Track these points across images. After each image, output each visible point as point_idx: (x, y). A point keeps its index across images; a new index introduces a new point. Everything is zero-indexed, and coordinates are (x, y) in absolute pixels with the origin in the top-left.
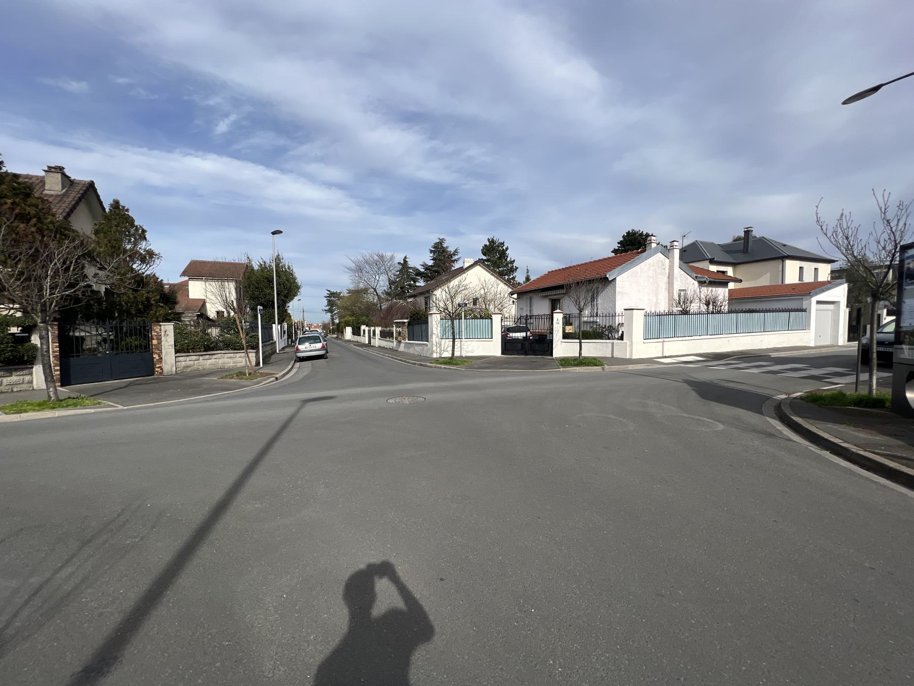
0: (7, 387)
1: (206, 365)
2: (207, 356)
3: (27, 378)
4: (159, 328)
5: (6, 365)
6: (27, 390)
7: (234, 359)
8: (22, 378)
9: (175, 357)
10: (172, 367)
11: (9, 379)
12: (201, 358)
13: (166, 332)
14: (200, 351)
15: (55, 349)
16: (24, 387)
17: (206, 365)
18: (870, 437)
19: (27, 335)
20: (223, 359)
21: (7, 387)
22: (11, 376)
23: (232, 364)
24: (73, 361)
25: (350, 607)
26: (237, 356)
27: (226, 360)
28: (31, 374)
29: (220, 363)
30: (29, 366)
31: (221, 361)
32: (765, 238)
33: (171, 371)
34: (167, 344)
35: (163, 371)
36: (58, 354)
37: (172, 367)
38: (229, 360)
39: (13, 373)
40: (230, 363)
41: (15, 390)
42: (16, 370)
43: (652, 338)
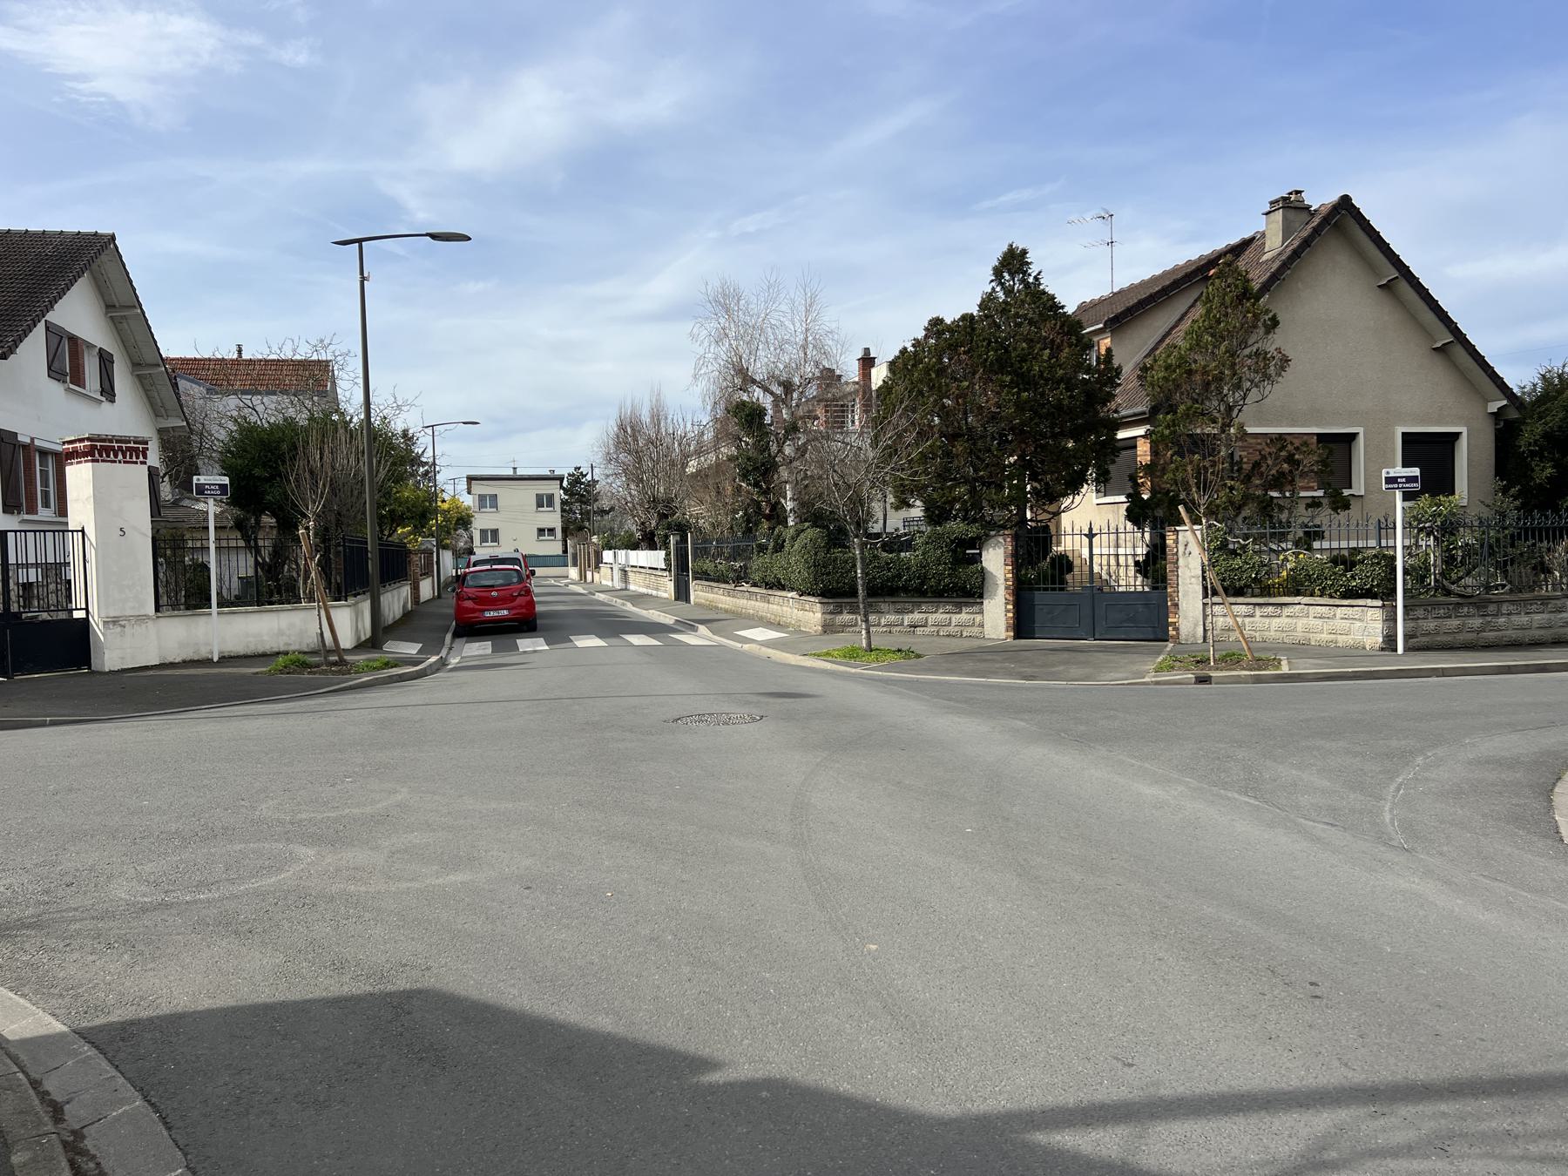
0: (957, 629)
1: (1269, 629)
2: (1271, 609)
3: (978, 618)
4: (1174, 537)
5: (935, 597)
6: (977, 637)
7: (1331, 622)
8: (972, 616)
9: (15, 445)
10: (1196, 625)
11: (958, 616)
12: (1258, 611)
13: (1186, 545)
14: (1253, 596)
15: (1008, 576)
16: (975, 630)
17: (1269, 629)
18: (644, 613)
19: (978, 551)
20: (1305, 621)
21: (957, 629)
22: (960, 613)
23: (1325, 637)
24: (1040, 597)
25: (945, 1123)
26: (1338, 616)
27: (1313, 622)
28: (981, 612)
29: (1299, 629)
30: (978, 600)
31: (1301, 624)
32: (172, 665)
33: (1194, 636)
34: (1188, 573)
35: (1178, 634)
36: (1011, 583)
37: (1196, 625)
38: (1319, 622)
39: (964, 608)
40: (1322, 632)
41: (965, 634)
42: (967, 604)
43: (23, 533)
